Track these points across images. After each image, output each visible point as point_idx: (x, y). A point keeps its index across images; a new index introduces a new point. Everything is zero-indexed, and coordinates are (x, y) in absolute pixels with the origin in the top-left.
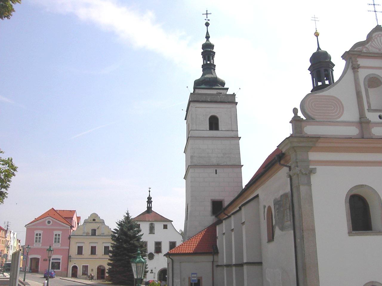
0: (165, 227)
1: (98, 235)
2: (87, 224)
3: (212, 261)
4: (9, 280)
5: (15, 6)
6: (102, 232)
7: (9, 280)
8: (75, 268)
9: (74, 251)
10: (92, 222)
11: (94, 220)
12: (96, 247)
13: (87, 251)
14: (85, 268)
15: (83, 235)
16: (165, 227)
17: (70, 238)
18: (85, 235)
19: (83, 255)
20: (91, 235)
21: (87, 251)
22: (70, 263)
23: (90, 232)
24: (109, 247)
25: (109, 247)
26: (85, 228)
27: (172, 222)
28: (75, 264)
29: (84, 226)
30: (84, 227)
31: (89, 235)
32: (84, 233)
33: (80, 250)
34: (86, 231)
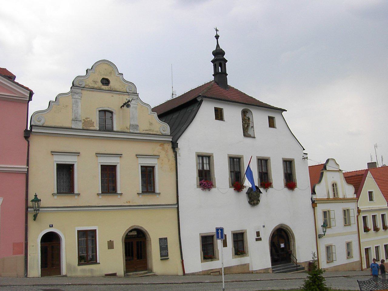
0: (272, 123)
1: (119, 130)
2: (86, 94)
3: (119, 158)
4: (220, 71)
5: (46, 81)
6: (132, 123)
7: (220, 71)
8: (51, 241)
9: (44, 182)
10: (100, 89)
11: (106, 82)
12: (260, 232)
13: (88, 179)
14: (87, 238)
15: (73, 127)
16: (272, 123)
17: (27, 135)
18: (81, 128)
19: (78, 195)
20: (98, 128)
21: (88, 179)
22: (32, 224)
23: (95, 119)
24: (326, 212)
25: (326, 212)
26: (80, 104)
27: (284, 113)
28: (51, 226)
29: (76, 96)
30: (77, 102)
31: (92, 128)
32: (75, 120)
33: (66, 172)
34: (82, 114)
